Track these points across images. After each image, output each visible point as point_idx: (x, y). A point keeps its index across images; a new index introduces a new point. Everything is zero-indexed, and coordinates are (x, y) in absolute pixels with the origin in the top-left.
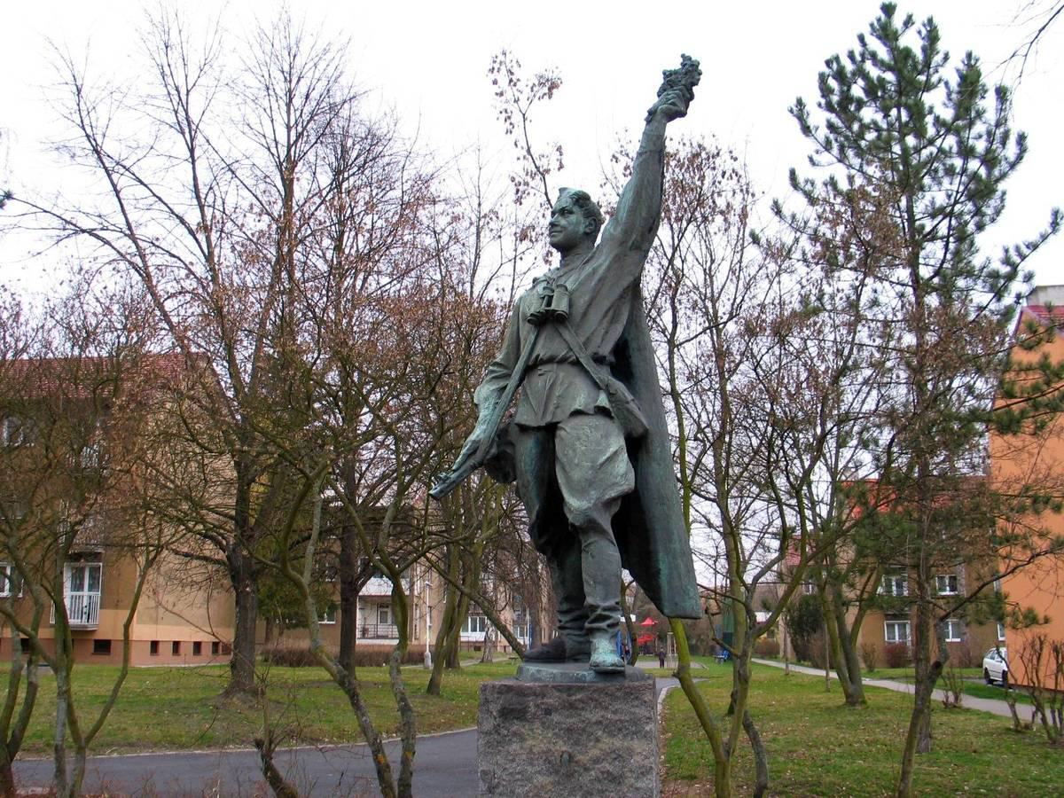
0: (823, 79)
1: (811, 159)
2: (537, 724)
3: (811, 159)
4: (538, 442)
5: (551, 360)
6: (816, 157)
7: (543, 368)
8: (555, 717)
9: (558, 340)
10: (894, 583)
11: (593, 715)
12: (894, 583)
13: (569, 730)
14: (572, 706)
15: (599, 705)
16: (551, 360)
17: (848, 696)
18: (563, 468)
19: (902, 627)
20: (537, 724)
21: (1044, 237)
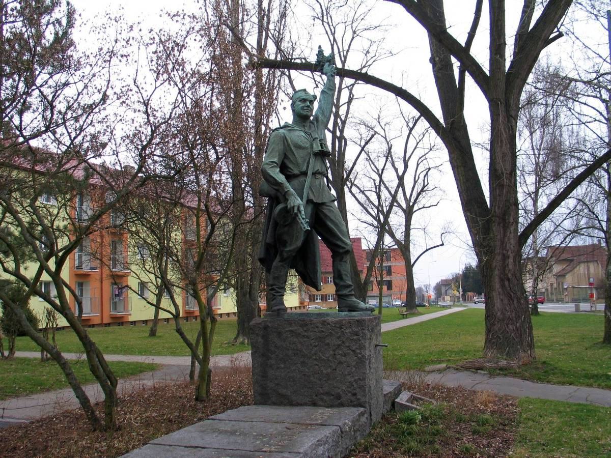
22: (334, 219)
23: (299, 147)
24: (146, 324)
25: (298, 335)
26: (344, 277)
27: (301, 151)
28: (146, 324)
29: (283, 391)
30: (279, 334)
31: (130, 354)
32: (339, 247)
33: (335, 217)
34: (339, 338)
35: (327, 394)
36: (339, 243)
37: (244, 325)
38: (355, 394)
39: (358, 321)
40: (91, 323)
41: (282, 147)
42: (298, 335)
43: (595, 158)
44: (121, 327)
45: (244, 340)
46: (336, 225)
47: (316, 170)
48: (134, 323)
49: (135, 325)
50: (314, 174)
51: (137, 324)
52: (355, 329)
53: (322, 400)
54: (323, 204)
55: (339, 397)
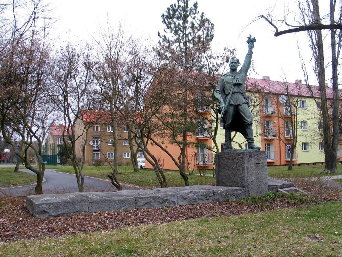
0: (169, 9)
1: (165, 30)
2: (253, 158)
3: (165, 30)
4: (234, 108)
5: (238, 92)
6: (166, 30)
7: (236, 94)
8: (256, 157)
9: (239, 89)
10: (96, 141)
11: (260, 156)
12: (96, 141)
13: (257, 159)
14: (258, 155)
15: (261, 155)
16: (238, 92)
17: (135, 169)
18: (242, 112)
19: (98, 154)
20: (253, 158)
21: (108, 17)
22: (243, 111)
23: (228, 83)
24: (322, 164)
25: (227, 158)
26: (249, 135)
27: (229, 84)
28: (322, 164)
29: (223, 181)
30: (222, 158)
31: (291, 187)
32: (245, 122)
33: (243, 110)
34: (238, 159)
35: (235, 182)
36: (245, 121)
37: (328, 163)
38: (242, 183)
39: (243, 152)
40: (275, 164)
41: (222, 84)
42: (227, 158)
43: (278, 97)
44: (300, 166)
45: (328, 172)
46: (244, 113)
47: (234, 91)
48: (300, 165)
49: (308, 165)
50: (233, 93)
51: (309, 165)
52: (242, 156)
53: (233, 184)
54: (239, 105)
55: (238, 184)
